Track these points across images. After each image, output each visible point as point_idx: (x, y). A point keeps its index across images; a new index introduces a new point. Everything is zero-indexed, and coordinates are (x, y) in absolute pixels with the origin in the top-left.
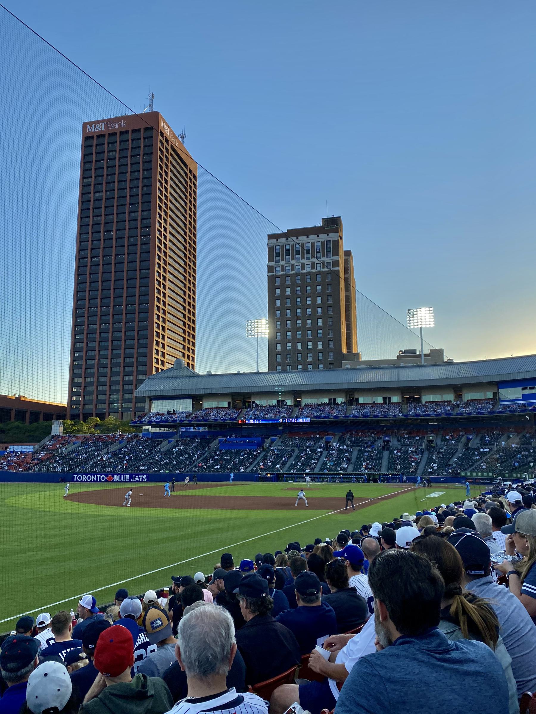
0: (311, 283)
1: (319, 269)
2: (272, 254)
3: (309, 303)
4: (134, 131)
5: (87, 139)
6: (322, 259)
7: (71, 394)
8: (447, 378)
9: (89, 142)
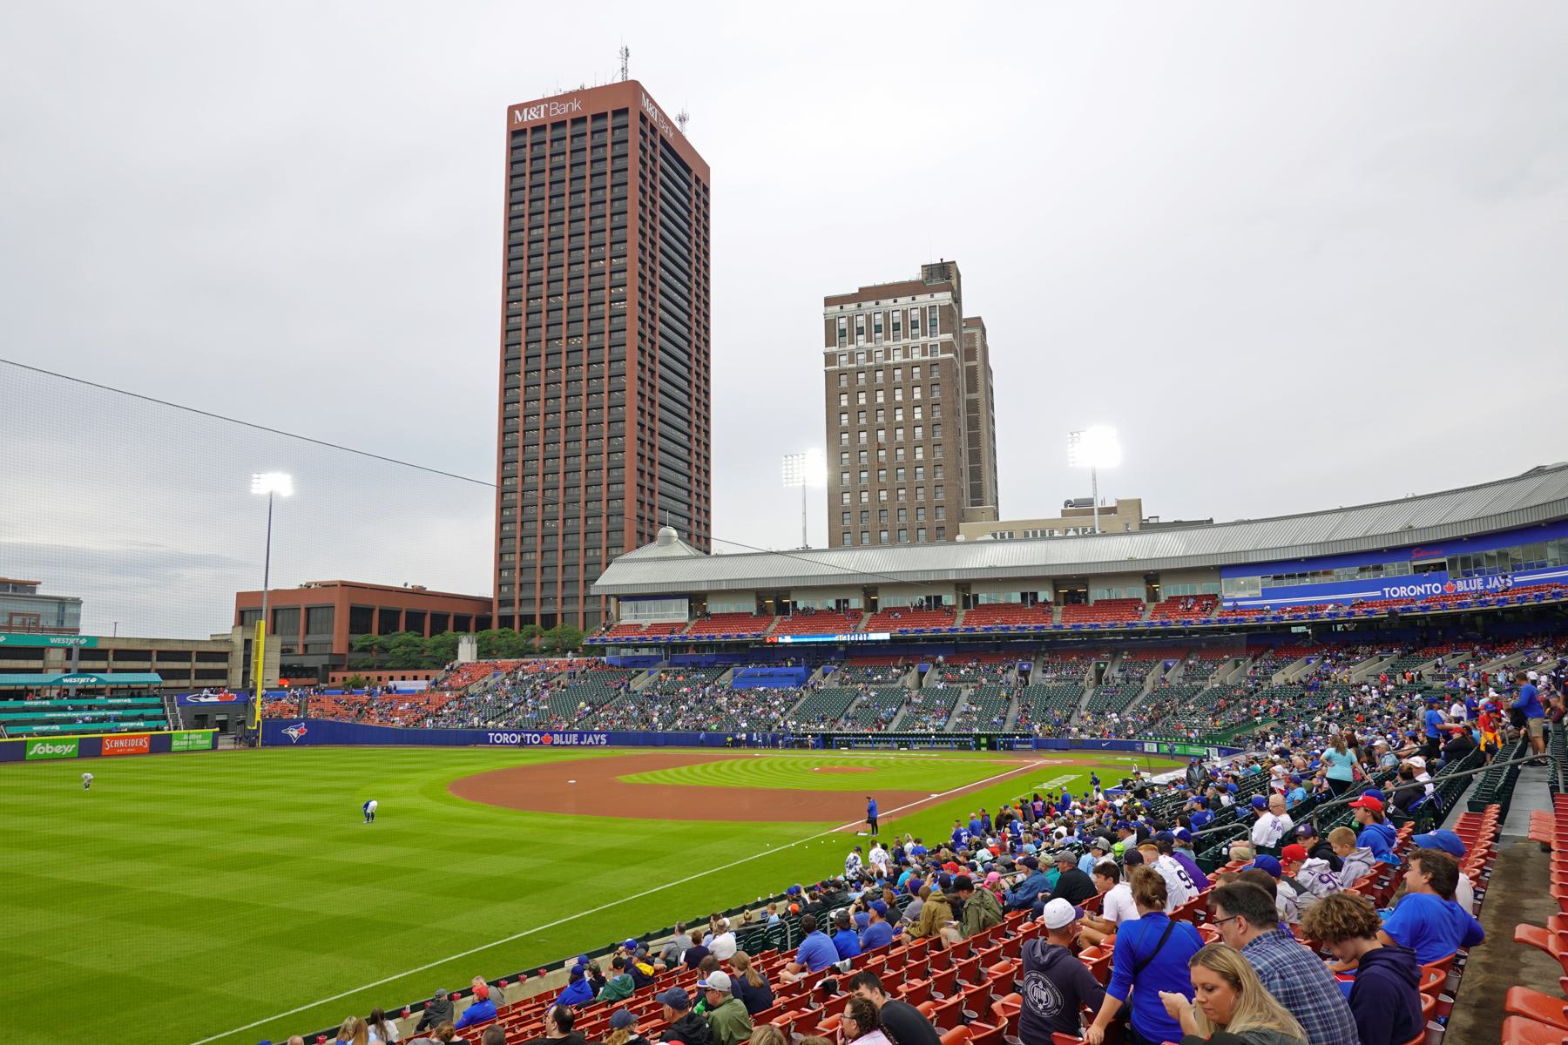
0: (917, 379)
1: (917, 356)
2: (833, 333)
3: (899, 418)
4: (595, 117)
5: (515, 133)
6: (922, 339)
7: (499, 586)
8: (1131, 560)
9: (519, 141)
